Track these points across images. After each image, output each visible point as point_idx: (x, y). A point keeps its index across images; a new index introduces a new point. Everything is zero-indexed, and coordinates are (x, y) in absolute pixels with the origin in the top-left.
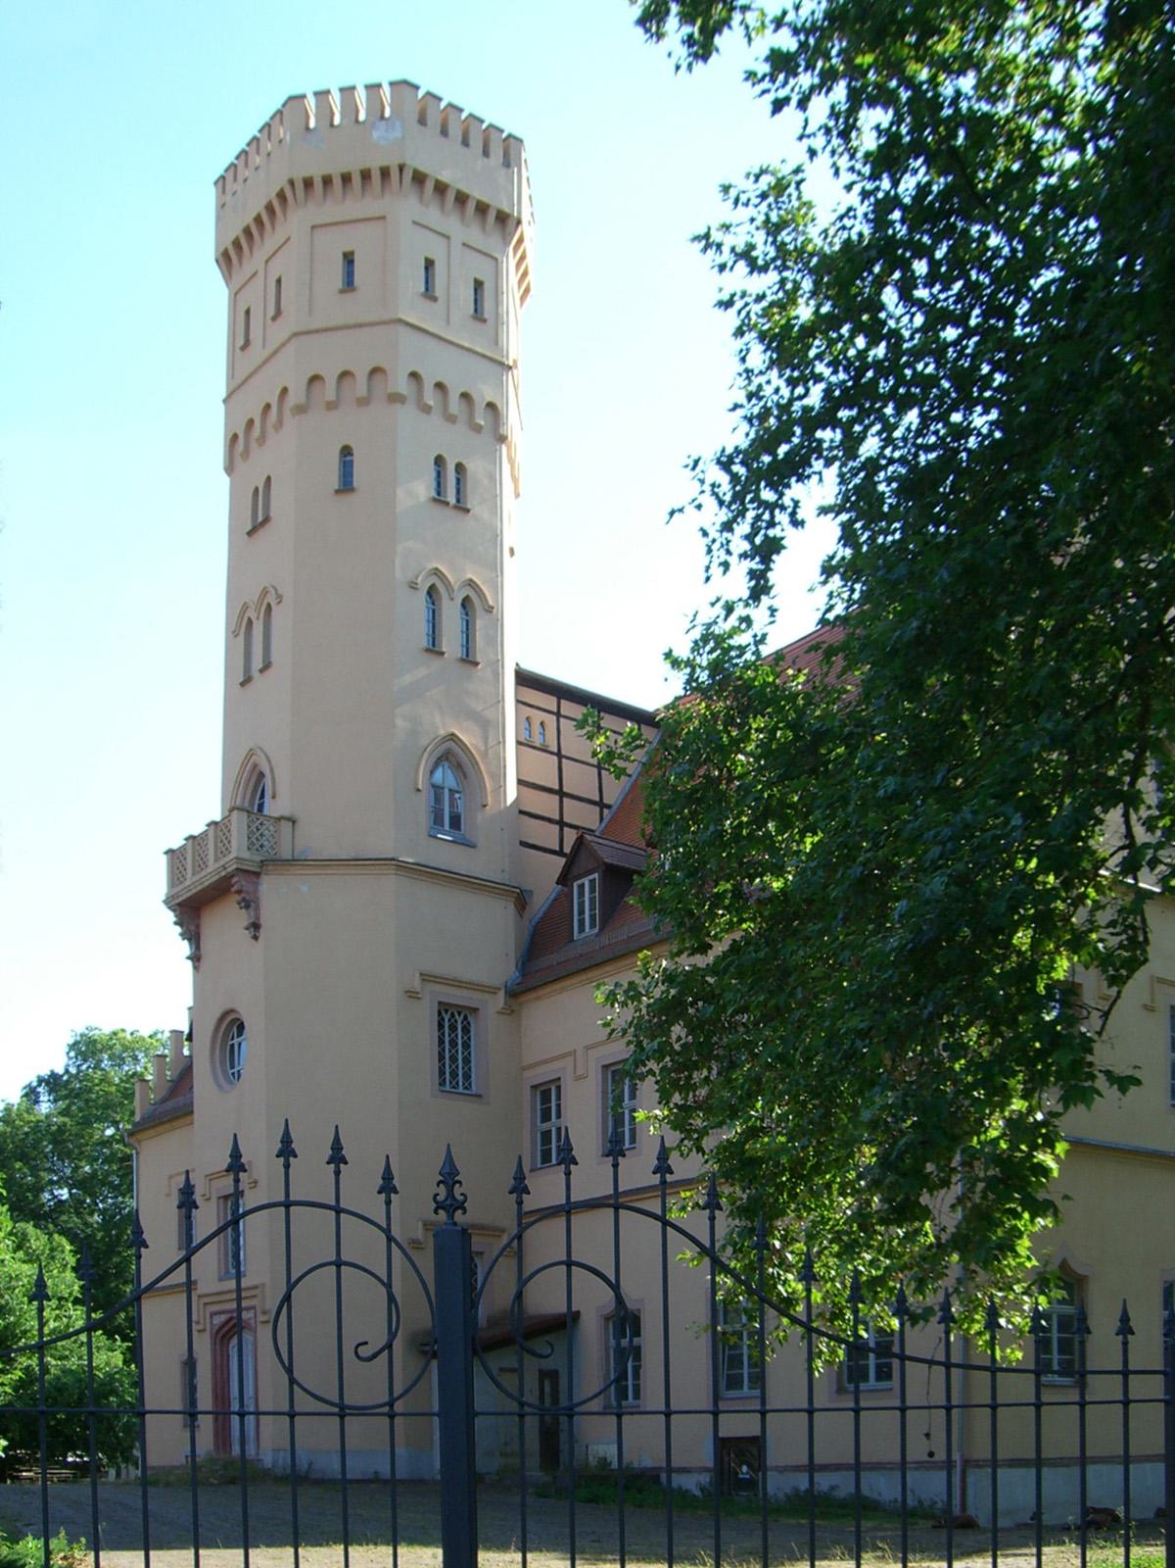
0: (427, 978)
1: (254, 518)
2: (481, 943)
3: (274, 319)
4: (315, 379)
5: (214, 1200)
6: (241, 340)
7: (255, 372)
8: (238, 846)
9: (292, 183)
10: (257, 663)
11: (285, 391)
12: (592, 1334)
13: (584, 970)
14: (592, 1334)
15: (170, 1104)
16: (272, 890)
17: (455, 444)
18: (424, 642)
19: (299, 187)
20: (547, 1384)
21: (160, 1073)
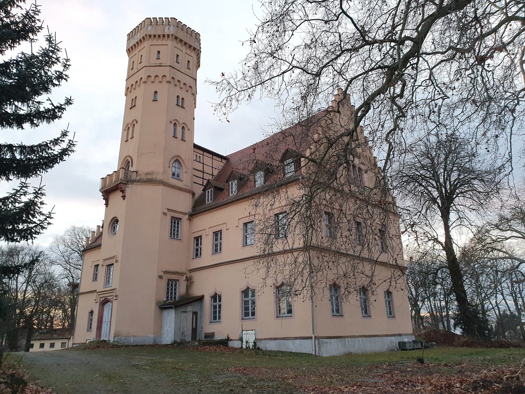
0: (166, 272)
1: (132, 105)
2: (184, 203)
4: (149, 76)
5: (105, 266)
6: (131, 67)
8: (121, 176)
9: (146, 35)
10: (130, 136)
11: (142, 78)
12: (207, 302)
13: (209, 210)
14: (207, 302)
15: (94, 244)
16: (130, 190)
18: (173, 135)
19: (148, 36)
20: (194, 316)
21: (93, 235)
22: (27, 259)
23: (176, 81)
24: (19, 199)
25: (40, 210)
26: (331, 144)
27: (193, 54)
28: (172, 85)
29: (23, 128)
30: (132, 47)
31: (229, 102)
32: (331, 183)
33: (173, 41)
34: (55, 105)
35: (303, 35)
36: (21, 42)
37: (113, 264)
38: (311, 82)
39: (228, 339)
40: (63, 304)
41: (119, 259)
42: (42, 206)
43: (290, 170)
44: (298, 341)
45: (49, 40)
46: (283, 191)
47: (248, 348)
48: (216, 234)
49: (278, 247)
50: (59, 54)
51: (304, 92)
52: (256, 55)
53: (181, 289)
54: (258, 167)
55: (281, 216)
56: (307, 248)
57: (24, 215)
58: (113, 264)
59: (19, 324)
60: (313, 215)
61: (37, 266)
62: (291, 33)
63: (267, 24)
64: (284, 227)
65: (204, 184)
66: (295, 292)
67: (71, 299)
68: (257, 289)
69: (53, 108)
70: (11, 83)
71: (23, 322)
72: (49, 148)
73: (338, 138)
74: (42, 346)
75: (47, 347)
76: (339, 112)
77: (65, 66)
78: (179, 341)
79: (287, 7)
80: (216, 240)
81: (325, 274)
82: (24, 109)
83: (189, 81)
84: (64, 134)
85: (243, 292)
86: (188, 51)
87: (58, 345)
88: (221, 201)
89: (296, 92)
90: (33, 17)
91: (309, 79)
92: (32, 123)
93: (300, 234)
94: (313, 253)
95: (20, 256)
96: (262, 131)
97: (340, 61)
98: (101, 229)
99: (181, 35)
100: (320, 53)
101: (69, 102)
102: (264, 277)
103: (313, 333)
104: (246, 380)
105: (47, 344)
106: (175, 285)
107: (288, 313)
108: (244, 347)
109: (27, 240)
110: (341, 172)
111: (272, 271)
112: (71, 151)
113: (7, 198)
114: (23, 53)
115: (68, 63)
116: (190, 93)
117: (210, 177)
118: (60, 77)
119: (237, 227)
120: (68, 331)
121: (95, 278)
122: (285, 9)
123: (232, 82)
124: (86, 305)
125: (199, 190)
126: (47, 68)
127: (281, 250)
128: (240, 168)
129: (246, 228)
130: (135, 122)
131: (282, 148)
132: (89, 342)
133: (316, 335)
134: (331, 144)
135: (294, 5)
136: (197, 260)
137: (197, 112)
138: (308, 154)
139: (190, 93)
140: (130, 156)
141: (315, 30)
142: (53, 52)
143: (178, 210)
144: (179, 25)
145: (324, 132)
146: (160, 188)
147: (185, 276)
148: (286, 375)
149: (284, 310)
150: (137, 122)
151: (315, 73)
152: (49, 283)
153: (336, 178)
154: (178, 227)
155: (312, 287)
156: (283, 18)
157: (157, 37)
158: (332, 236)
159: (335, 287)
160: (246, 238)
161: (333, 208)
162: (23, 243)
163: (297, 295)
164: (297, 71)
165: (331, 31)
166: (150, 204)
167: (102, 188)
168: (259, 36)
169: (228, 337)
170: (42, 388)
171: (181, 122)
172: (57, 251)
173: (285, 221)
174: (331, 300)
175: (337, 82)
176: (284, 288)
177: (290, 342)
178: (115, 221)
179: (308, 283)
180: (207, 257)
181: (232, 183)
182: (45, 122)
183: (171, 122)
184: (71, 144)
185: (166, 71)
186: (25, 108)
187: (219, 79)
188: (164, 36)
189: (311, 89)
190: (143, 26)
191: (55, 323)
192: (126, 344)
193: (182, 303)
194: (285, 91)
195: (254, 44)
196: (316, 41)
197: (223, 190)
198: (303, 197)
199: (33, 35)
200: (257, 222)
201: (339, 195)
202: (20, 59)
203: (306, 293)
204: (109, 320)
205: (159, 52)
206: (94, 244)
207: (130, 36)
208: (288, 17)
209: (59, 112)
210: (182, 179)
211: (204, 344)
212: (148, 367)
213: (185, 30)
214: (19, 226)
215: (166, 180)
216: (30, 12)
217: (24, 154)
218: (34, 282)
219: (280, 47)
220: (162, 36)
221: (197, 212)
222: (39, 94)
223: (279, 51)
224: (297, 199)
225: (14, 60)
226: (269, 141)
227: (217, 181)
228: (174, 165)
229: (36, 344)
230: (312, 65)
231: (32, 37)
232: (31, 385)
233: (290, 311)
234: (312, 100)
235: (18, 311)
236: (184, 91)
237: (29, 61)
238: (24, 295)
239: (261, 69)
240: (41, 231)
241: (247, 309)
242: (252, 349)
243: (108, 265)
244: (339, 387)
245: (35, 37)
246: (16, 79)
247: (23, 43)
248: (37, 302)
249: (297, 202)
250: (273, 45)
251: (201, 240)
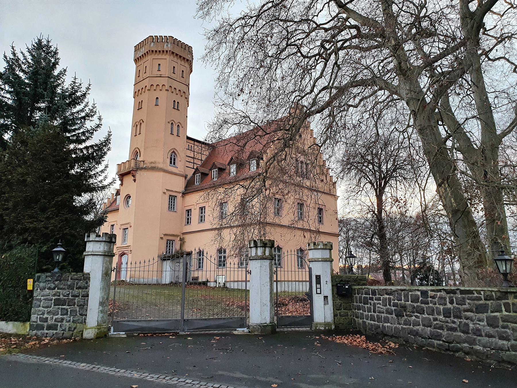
0: (165, 235)
2: (179, 184)
8: (133, 164)
10: (138, 133)
12: (194, 256)
16: (138, 175)
17: (178, 99)
19: (151, 51)
23: (173, 88)
27: (187, 65)
28: (170, 92)
33: (170, 56)
39: (208, 281)
41: (132, 225)
48: (201, 209)
53: (177, 246)
80: (202, 213)
83: (183, 88)
86: (183, 63)
106: (172, 244)
116: (183, 97)
125: (190, 173)
130: (141, 121)
136: (188, 226)
144: (176, 42)
154: (174, 202)
157: (158, 52)
180: (195, 225)
183: (169, 122)
188: (163, 51)
190: (147, 42)
205: (159, 65)
207: (137, 48)
211: (191, 284)
215: (166, 168)
220: (161, 52)
221: (189, 191)
236: (179, 95)
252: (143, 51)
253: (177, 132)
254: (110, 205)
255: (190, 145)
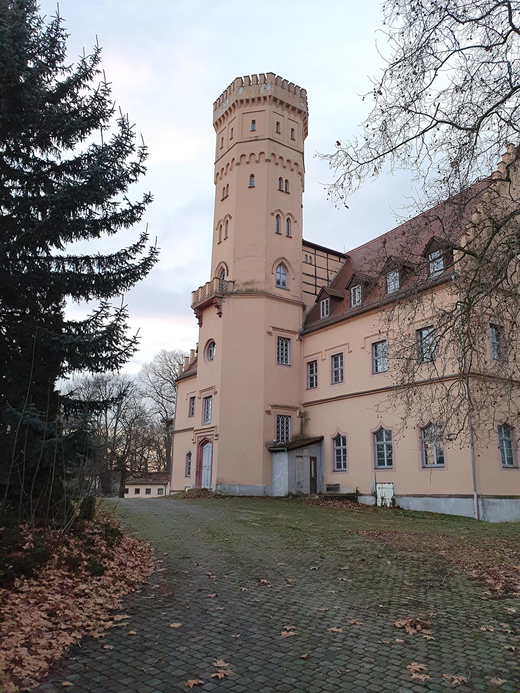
0: (275, 406)
1: (223, 196)
2: (292, 319)
3: (230, 140)
4: (243, 155)
5: (202, 399)
6: (220, 147)
7: (225, 154)
8: (216, 288)
10: (223, 237)
11: (234, 159)
12: (328, 443)
13: (324, 327)
15: (189, 372)
16: (227, 305)
17: (286, 175)
18: (275, 231)
19: (239, 102)
21: (187, 362)
22: (115, 395)
24: (101, 323)
25: (124, 335)
26: (497, 227)
27: (298, 119)
28: (272, 164)
29: (99, 237)
30: (220, 120)
31: (347, 180)
32: (499, 284)
34: (133, 205)
35: (452, 73)
36: (91, 131)
37: (211, 396)
38: (465, 141)
40: (158, 444)
41: (218, 390)
42: (126, 330)
43: (437, 267)
44: (452, 500)
45: (123, 124)
46: (426, 299)
47: (384, 506)
48: (335, 357)
49: (423, 374)
50: (133, 141)
51: (455, 155)
52: (383, 112)
53: (294, 429)
54: (390, 264)
55: (425, 333)
56: (463, 376)
57: (107, 342)
58: (211, 396)
59: (111, 465)
60: (473, 331)
61: (126, 400)
62: (433, 72)
63: (398, 65)
64: (430, 349)
65: (318, 293)
66: (449, 435)
67: (166, 438)
68: (395, 431)
69: (131, 208)
70: (83, 184)
71: (115, 464)
72: (130, 257)
73: (507, 219)
74: (137, 491)
75: (143, 494)
76: (508, 180)
77: (141, 156)
78: (294, 493)
79: (427, 35)
80: (336, 366)
81: (491, 412)
82: (99, 213)
83: (293, 156)
84: (144, 238)
85: (375, 433)
86: (292, 116)
87: (154, 493)
88: (339, 315)
89: (442, 157)
90: (103, 98)
91: (462, 136)
92: (109, 229)
93: (453, 358)
94: (473, 383)
95: (108, 387)
96: (394, 215)
97: (510, 104)
98: (196, 354)
99: (282, 95)
100: (478, 96)
101: (148, 199)
102: (403, 416)
103: (475, 491)
104: (382, 548)
105: (143, 489)
106: (287, 423)
107: (438, 462)
108: (379, 504)
109: (112, 370)
110: (514, 267)
111: (415, 408)
112: (154, 260)
113: (88, 322)
114: (94, 145)
115: (145, 152)
116: (295, 173)
117: (325, 284)
118: (137, 170)
119: (362, 348)
120: (164, 476)
121: (192, 413)
122: (424, 39)
123: (351, 152)
124: (183, 445)
125: (310, 302)
126: (121, 161)
127: (426, 379)
128: (365, 269)
129: (376, 349)
130: (228, 218)
131: (425, 238)
132: (189, 490)
133: (478, 494)
134: (497, 227)
135: (437, 31)
136: (313, 392)
137: (307, 197)
138: (463, 242)
139: (295, 173)
140: (224, 262)
141: (469, 63)
142: (126, 139)
143: (286, 328)
145: (488, 211)
146: (262, 301)
147: (298, 411)
148: (437, 545)
149: (433, 459)
150: (230, 217)
151: (471, 127)
152: (140, 418)
153: (506, 277)
155: (472, 429)
156: (422, 52)
157: (251, 101)
158: (502, 358)
159: (506, 428)
160: (376, 361)
161: (502, 319)
162: (108, 372)
163: (451, 440)
164: (444, 127)
165: (496, 60)
166: (252, 320)
167: (194, 304)
168: (387, 83)
169: (357, 491)
170: (139, 541)
171: (285, 212)
172: (146, 381)
173: (431, 340)
174: (500, 447)
175: (505, 136)
176: (432, 429)
177: (442, 502)
178: (211, 344)
179: (466, 425)
180: (325, 388)
181: (354, 290)
182: (123, 227)
183: (272, 214)
184: (154, 252)
185: (263, 146)
186: (100, 212)
187: (334, 150)
189: (466, 151)
190: (232, 89)
191: (149, 465)
192: (230, 494)
193: (296, 445)
194: (427, 157)
195: (380, 96)
196: (472, 79)
197: (343, 299)
198: (456, 305)
199: (104, 120)
200: (391, 342)
201: (510, 300)
202: (91, 153)
203: (465, 437)
204: (210, 465)
205: (254, 122)
206: (188, 373)
207: (217, 105)
208: (429, 51)
209: (138, 212)
210: (289, 288)
211: (326, 498)
212: (258, 525)
213: (286, 87)
214: (103, 355)
215: (270, 291)
216: (99, 92)
217: (102, 266)
218: (124, 417)
219: (417, 96)
220: (256, 100)
222: (114, 193)
223: (417, 103)
224: (448, 309)
225: (86, 154)
226: (405, 230)
227: (333, 288)
228: (278, 270)
229: (131, 489)
230: (466, 116)
231: (103, 124)
232: (127, 538)
233: (441, 460)
234: (467, 166)
235: (109, 451)
236: (288, 170)
237: (101, 154)
238: (115, 433)
239: (392, 130)
240: (127, 359)
241: (380, 455)
242: (390, 508)
243: (206, 398)
244: (515, 567)
245: (107, 124)
246: (88, 178)
247: (94, 131)
248: (128, 441)
249: (448, 313)
250: (406, 94)
251: (316, 366)
252: (228, 104)
253: (286, 230)
254: (190, 368)
255: (309, 255)
